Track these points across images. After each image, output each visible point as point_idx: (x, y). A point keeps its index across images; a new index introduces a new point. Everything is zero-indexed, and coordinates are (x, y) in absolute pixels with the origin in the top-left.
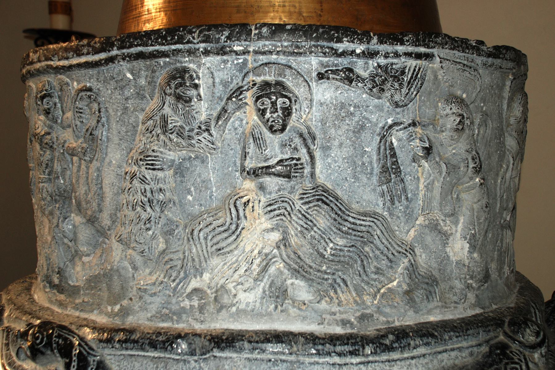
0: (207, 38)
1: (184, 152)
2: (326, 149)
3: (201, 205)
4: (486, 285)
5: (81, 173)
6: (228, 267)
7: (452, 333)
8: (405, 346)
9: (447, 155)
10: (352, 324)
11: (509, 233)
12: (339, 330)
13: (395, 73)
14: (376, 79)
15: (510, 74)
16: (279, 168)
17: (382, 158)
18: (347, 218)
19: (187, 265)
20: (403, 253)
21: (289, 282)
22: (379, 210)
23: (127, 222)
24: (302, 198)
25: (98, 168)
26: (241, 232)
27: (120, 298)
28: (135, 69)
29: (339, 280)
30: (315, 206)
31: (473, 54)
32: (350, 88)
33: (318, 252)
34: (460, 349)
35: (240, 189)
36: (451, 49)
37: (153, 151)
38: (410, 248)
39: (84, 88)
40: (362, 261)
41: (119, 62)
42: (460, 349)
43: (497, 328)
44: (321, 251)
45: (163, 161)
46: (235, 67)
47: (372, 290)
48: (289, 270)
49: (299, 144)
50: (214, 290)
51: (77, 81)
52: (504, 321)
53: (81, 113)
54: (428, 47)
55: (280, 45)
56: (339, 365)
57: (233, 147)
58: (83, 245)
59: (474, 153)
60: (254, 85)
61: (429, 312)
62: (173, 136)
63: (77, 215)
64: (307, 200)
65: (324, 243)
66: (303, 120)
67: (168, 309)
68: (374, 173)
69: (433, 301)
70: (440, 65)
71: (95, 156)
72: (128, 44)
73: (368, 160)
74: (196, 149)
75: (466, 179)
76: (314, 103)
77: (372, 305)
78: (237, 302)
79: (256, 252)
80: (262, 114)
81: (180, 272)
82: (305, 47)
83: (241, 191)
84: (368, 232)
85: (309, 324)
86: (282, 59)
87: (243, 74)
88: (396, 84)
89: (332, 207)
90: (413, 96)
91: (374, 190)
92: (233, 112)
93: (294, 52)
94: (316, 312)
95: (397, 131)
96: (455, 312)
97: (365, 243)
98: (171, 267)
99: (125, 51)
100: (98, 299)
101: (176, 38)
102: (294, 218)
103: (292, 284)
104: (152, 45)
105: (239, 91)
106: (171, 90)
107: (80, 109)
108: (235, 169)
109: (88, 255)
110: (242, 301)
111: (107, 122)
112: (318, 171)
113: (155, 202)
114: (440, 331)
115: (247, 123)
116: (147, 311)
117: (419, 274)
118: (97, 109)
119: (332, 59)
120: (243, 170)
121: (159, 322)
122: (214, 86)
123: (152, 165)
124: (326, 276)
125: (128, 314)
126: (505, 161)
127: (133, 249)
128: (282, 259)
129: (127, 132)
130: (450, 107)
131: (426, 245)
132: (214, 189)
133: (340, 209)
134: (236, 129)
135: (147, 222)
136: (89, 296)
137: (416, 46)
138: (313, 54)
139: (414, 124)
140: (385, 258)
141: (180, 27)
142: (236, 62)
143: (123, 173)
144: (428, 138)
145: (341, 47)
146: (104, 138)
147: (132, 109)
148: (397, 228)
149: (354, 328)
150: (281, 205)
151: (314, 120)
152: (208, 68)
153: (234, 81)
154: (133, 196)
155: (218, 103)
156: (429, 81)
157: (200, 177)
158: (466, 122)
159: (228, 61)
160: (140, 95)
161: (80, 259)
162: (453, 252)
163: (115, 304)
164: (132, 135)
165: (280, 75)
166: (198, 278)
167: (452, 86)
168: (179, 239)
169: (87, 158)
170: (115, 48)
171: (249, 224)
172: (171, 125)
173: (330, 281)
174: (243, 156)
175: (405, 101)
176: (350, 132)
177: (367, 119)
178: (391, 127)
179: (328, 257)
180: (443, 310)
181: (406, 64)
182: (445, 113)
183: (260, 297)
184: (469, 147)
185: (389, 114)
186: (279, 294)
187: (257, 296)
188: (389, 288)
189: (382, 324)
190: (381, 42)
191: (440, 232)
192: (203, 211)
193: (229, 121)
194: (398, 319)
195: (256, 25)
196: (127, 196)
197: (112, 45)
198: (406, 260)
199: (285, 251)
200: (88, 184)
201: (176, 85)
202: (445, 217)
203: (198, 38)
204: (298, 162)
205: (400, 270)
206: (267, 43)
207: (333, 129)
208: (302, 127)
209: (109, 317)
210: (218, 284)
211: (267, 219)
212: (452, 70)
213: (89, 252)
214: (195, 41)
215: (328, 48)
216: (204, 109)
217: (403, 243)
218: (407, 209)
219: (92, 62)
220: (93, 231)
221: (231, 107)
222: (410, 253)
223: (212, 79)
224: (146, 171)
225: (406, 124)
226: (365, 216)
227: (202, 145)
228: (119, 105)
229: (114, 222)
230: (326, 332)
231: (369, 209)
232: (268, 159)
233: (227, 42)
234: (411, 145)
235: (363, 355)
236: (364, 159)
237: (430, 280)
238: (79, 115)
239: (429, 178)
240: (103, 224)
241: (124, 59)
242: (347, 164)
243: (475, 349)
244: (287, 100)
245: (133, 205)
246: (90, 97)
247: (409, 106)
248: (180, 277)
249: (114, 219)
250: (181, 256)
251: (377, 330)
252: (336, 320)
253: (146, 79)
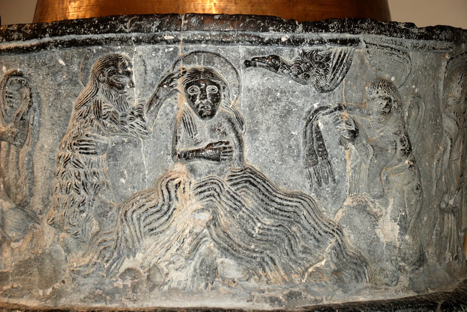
0: (138, 28)
1: (117, 137)
2: (253, 133)
3: (134, 187)
4: (422, 269)
5: (10, 158)
6: (160, 247)
9: (374, 138)
10: (280, 301)
11: (452, 217)
13: (320, 60)
14: (301, 66)
15: (447, 54)
16: (209, 152)
17: (308, 141)
18: (274, 198)
19: (120, 245)
20: (330, 233)
21: (219, 261)
22: (307, 192)
23: (60, 205)
24: (231, 180)
25: (29, 153)
26: (172, 212)
27: (52, 281)
28: (68, 56)
29: (267, 259)
30: (243, 187)
31: (401, 37)
32: (277, 75)
33: (247, 232)
35: (171, 172)
36: (378, 33)
37: (87, 135)
38: (337, 229)
39: (15, 73)
40: (289, 240)
41: (51, 48)
44: (249, 230)
45: (97, 146)
46: (166, 55)
47: (300, 269)
48: (219, 249)
49: (228, 129)
50: (147, 269)
51: (6, 65)
52: (437, 304)
53: (11, 97)
54: (354, 33)
55: (208, 34)
57: (165, 132)
58: (12, 230)
59: (403, 135)
60: (184, 72)
61: (358, 292)
62: (106, 122)
63: (5, 200)
64: (235, 182)
65: (252, 223)
66: (231, 106)
67: (101, 290)
68: (301, 155)
69: (362, 281)
70: (367, 50)
71: (25, 141)
72: (60, 31)
73: (295, 143)
74: (129, 134)
75: (395, 161)
76: (242, 89)
77: (300, 284)
78: (169, 281)
79: (187, 231)
80: (192, 100)
81: (113, 253)
82: (232, 36)
83: (172, 173)
84: (295, 212)
85: (238, 301)
86: (211, 48)
87: (174, 62)
88: (321, 70)
89: (259, 188)
90: (339, 80)
91: (301, 172)
92: (164, 98)
93: (222, 41)
94: (245, 289)
95: (323, 115)
96: (386, 293)
97: (292, 223)
98: (105, 248)
99: (57, 38)
100: (29, 283)
101: (109, 27)
102: (223, 198)
103: (222, 263)
104: (84, 33)
105: (170, 78)
106: (104, 78)
107: (10, 94)
108: (166, 152)
109: (17, 241)
110: (174, 279)
111: (39, 106)
112: (246, 154)
113: (89, 185)
114: (367, 310)
115: (178, 109)
116: (80, 293)
117: (347, 254)
118: (28, 94)
119: (258, 47)
120: (174, 153)
121: (92, 303)
122: (146, 73)
123: (86, 149)
124: (254, 255)
125: (61, 297)
126: (442, 143)
127: (67, 231)
128: (212, 238)
129: (60, 117)
130: (376, 91)
131: (354, 226)
132: (147, 172)
133: (267, 190)
134: (167, 114)
135: (81, 205)
136: (18, 282)
137: (341, 32)
138: (240, 43)
139: (340, 108)
140: (312, 237)
141: (112, 17)
142: (166, 50)
143: (56, 158)
144: (354, 122)
145: (267, 36)
146: (36, 123)
147: (65, 95)
148: (324, 209)
149: (282, 306)
150: (211, 186)
151: (242, 105)
152: (140, 56)
153: (165, 68)
154: (67, 179)
155: (150, 90)
156: (355, 66)
157: (133, 160)
158: (393, 106)
159: (159, 50)
160: (73, 82)
161: (9, 244)
162: (383, 233)
163: (47, 287)
164: (65, 120)
165: (209, 63)
166: (131, 258)
167: (379, 70)
168: (112, 221)
169: (18, 143)
170: (48, 35)
171: (181, 205)
172: (104, 111)
173: (258, 260)
174: (175, 141)
175: (331, 86)
176: (276, 117)
177: (293, 104)
178: (316, 111)
179: (257, 237)
180: (373, 291)
181: (331, 50)
182: (371, 96)
183: (191, 275)
184: (397, 130)
185: (315, 98)
186: (209, 272)
187: (188, 274)
188: (317, 268)
189: (310, 302)
190: (306, 30)
191: (369, 214)
192: (136, 193)
193: (160, 106)
194: (326, 298)
195: (186, 15)
196: (60, 180)
197: (44, 32)
198: (333, 240)
199: (215, 231)
200: (18, 169)
201: (109, 72)
202: (374, 198)
203: (130, 27)
204: (227, 146)
205: (327, 250)
206: (196, 32)
207: (260, 114)
208: (231, 113)
209: (41, 301)
210: (150, 263)
211: (198, 200)
212: (379, 54)
213: (18, 238)
214: (127, 31)
215: (255, 36)
216: (136, 96)
217: (330, 223)
218: (334, 190)
219: (23, 47)
220: (23, 217)
221: (162, 93)
222: (337, 233)
223: (144, 67)
224: (80, 155)
225: (332, 109)
226: (292, 197)
227: (135, 130)
228: (51, 91)
229: (46, 206)
230: (255, 309)
231: (296, 190)
232: (198, 143)
233: (157, 31)
234: (338, 128)
236: (291, 143)
237: (359, 260)
238: (8, 99)
239: (356, 160)
240: (34, 209)
241: (56, 46)
242: (274, 148)
244: (216, 87)
245: (67, 188)
246: (20, 82)
247: (335, 90)
248: (114, 257)
249: (46, 203)
250: (115, 237)
251: (305, 308)
252: (265, 298)
253: (78, 65)
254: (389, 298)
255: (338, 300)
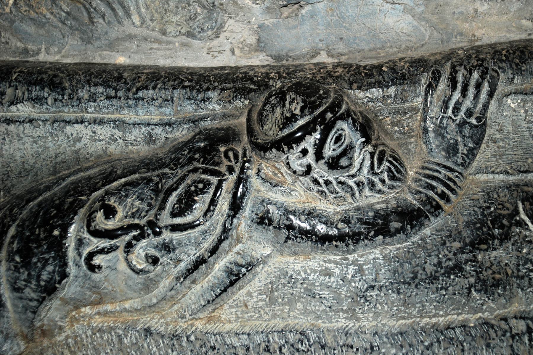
42: (120, 124)
243: (159, 130)
255: (75, 55)
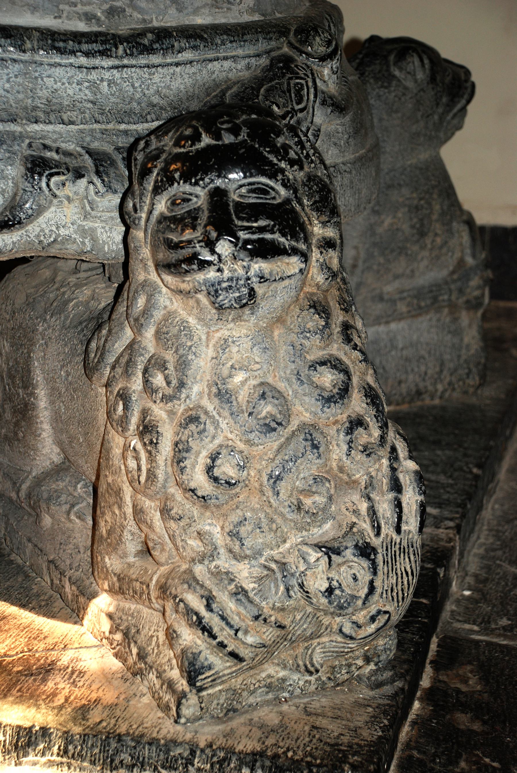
7: (225, 37)
8: (167, 48)
10: (98, 20)
12: (82, 27)
34: (234, 58)
42: (234, 58)
43: (280, 37)
52: (290, 30)
56: (86, 68)
85: (42, 17)
194: (156, 18)
235: (116, 57)
243: (253, 60)
251: (131, 29)
252: (78, 13)
254: (232, 21)
